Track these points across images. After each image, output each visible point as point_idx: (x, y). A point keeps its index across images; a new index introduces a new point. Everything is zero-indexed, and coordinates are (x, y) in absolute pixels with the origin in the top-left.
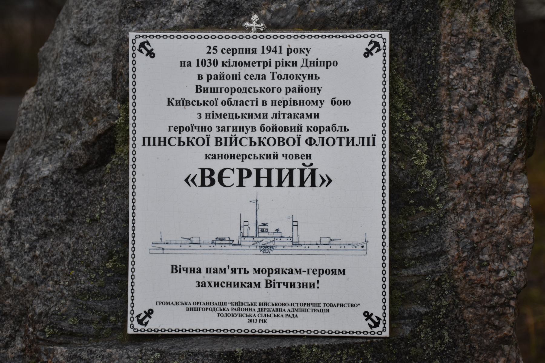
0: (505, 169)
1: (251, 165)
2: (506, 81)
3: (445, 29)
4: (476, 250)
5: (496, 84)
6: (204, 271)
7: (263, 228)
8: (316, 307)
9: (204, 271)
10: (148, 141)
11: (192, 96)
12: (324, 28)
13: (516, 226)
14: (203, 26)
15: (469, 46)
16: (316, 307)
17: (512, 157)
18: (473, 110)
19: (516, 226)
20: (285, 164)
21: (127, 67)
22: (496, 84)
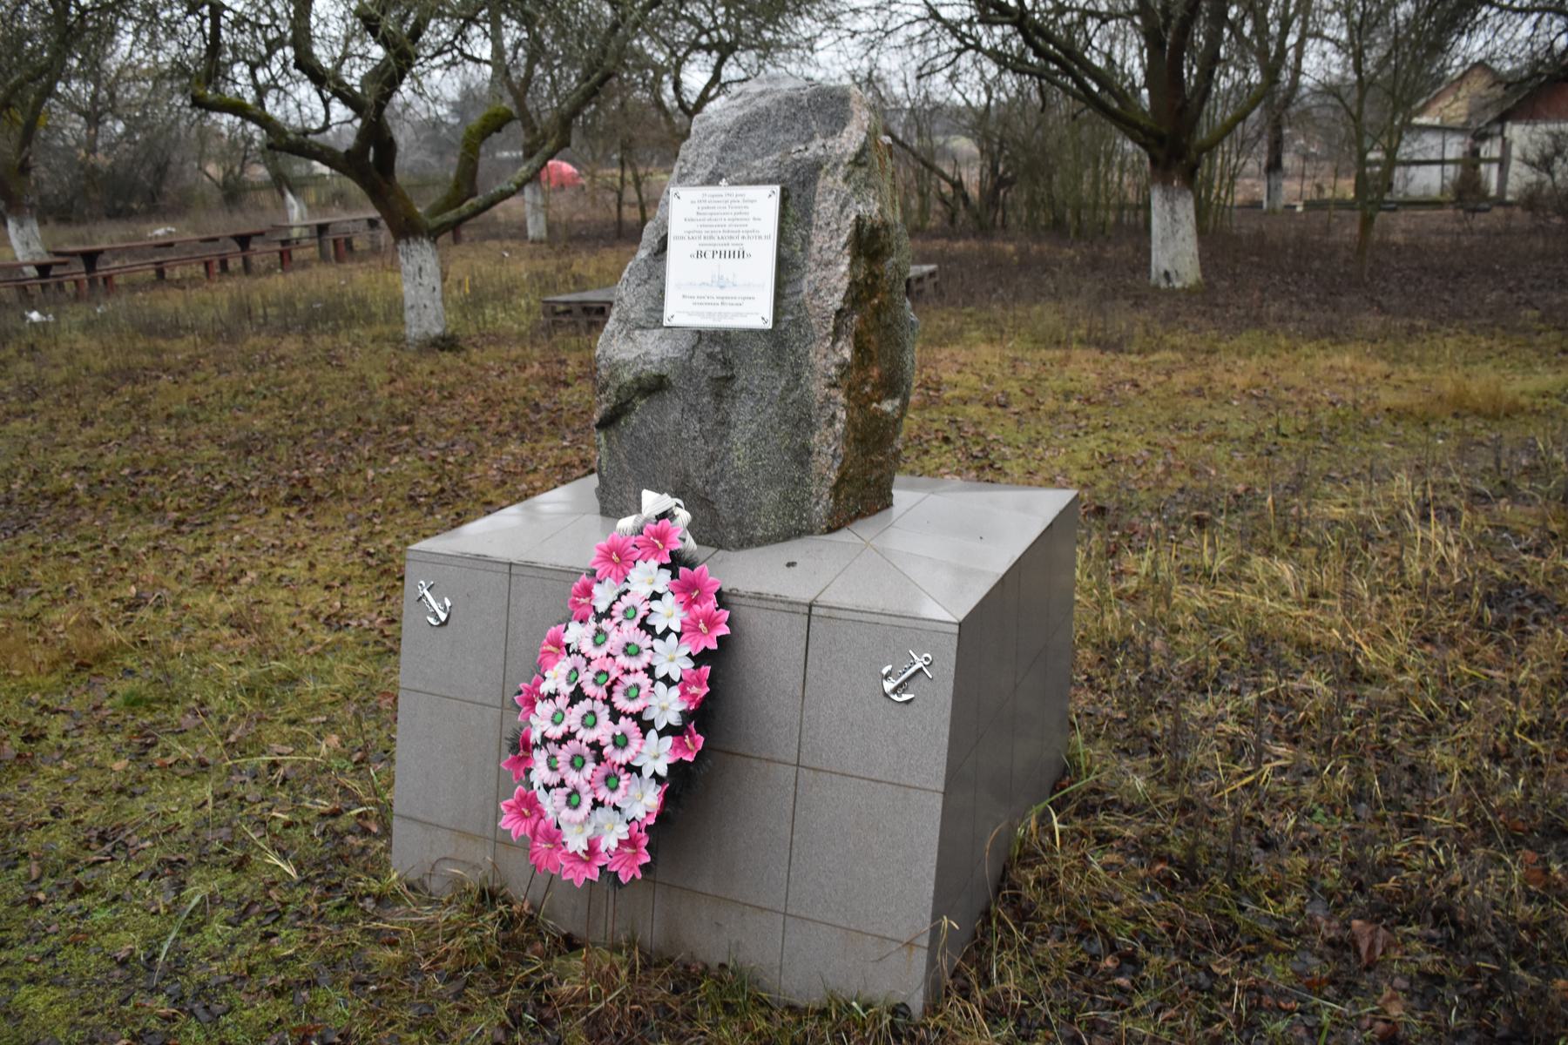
0: (839, 253)
1: (718, 249)
2: (847, 210)
3: (820, 184)
4: (817, 291)
5: (841, 212)
6: (709, 255)
7: (721, 278)
8: (741, 315)
9: (709, 255)
10: (676, 238)
11: (694, 216)
12: (777, 541)
13: (840, 280)
14: (505, 503)
15: (831, 192)
16: (741, 315)
17: (844, 248)
18: (828, 224)
19: (840, 280)
20: (732, 248)
21: (649, 235)
22: (841, 212)
